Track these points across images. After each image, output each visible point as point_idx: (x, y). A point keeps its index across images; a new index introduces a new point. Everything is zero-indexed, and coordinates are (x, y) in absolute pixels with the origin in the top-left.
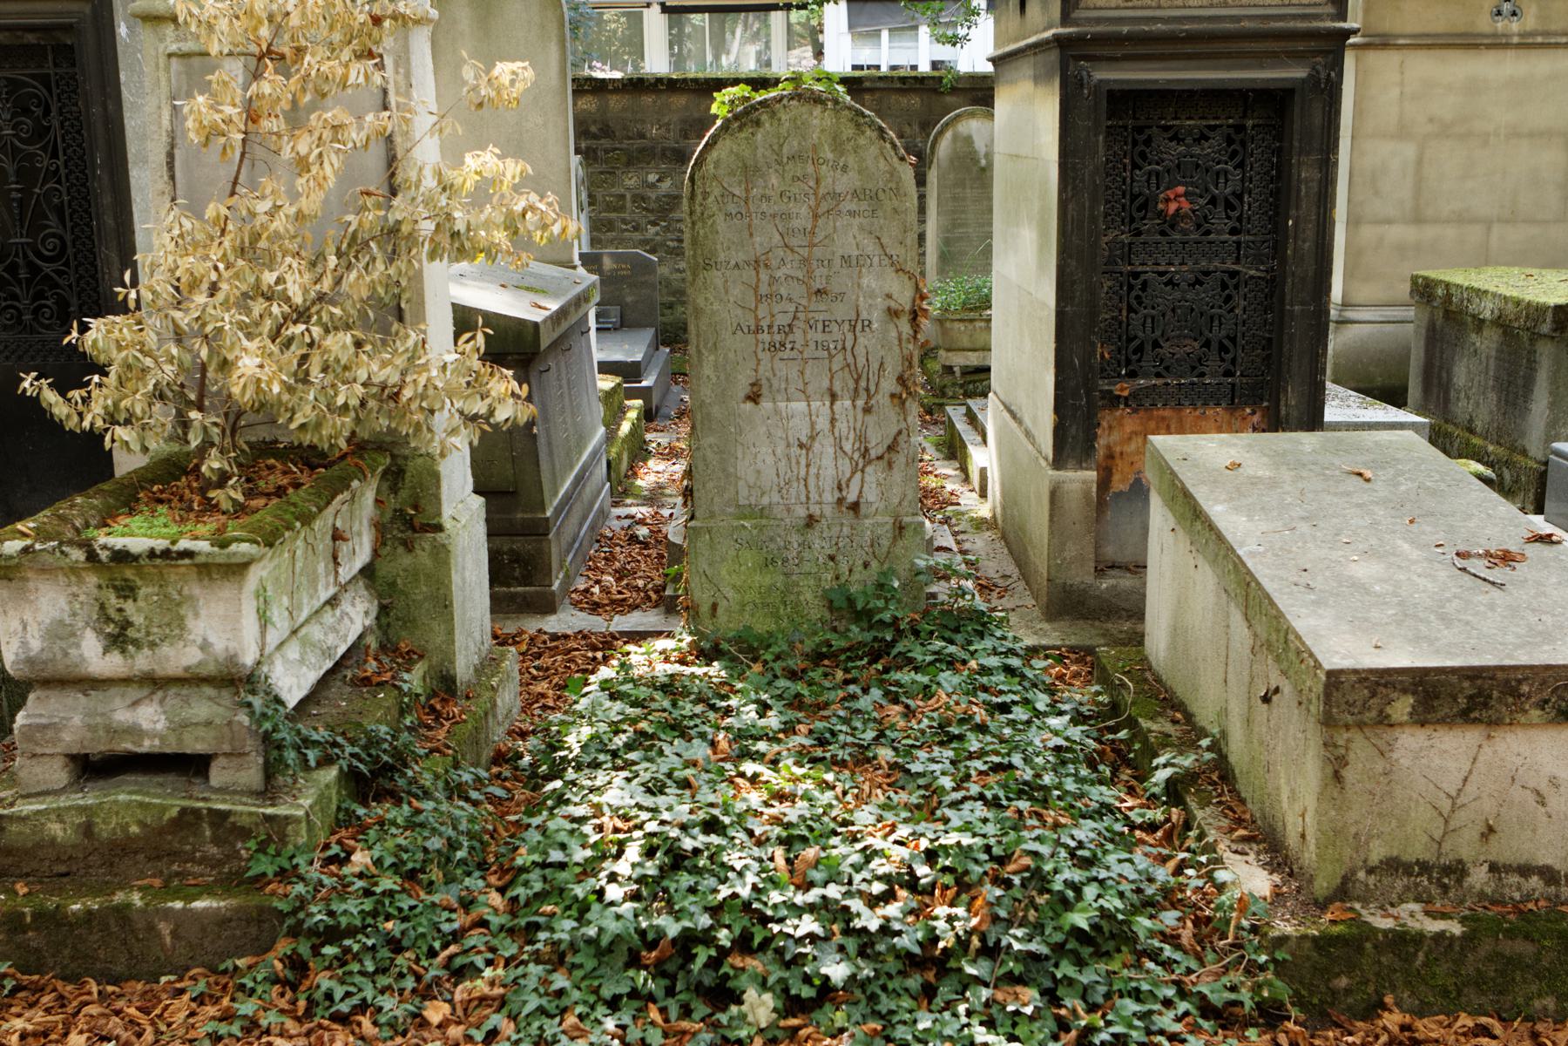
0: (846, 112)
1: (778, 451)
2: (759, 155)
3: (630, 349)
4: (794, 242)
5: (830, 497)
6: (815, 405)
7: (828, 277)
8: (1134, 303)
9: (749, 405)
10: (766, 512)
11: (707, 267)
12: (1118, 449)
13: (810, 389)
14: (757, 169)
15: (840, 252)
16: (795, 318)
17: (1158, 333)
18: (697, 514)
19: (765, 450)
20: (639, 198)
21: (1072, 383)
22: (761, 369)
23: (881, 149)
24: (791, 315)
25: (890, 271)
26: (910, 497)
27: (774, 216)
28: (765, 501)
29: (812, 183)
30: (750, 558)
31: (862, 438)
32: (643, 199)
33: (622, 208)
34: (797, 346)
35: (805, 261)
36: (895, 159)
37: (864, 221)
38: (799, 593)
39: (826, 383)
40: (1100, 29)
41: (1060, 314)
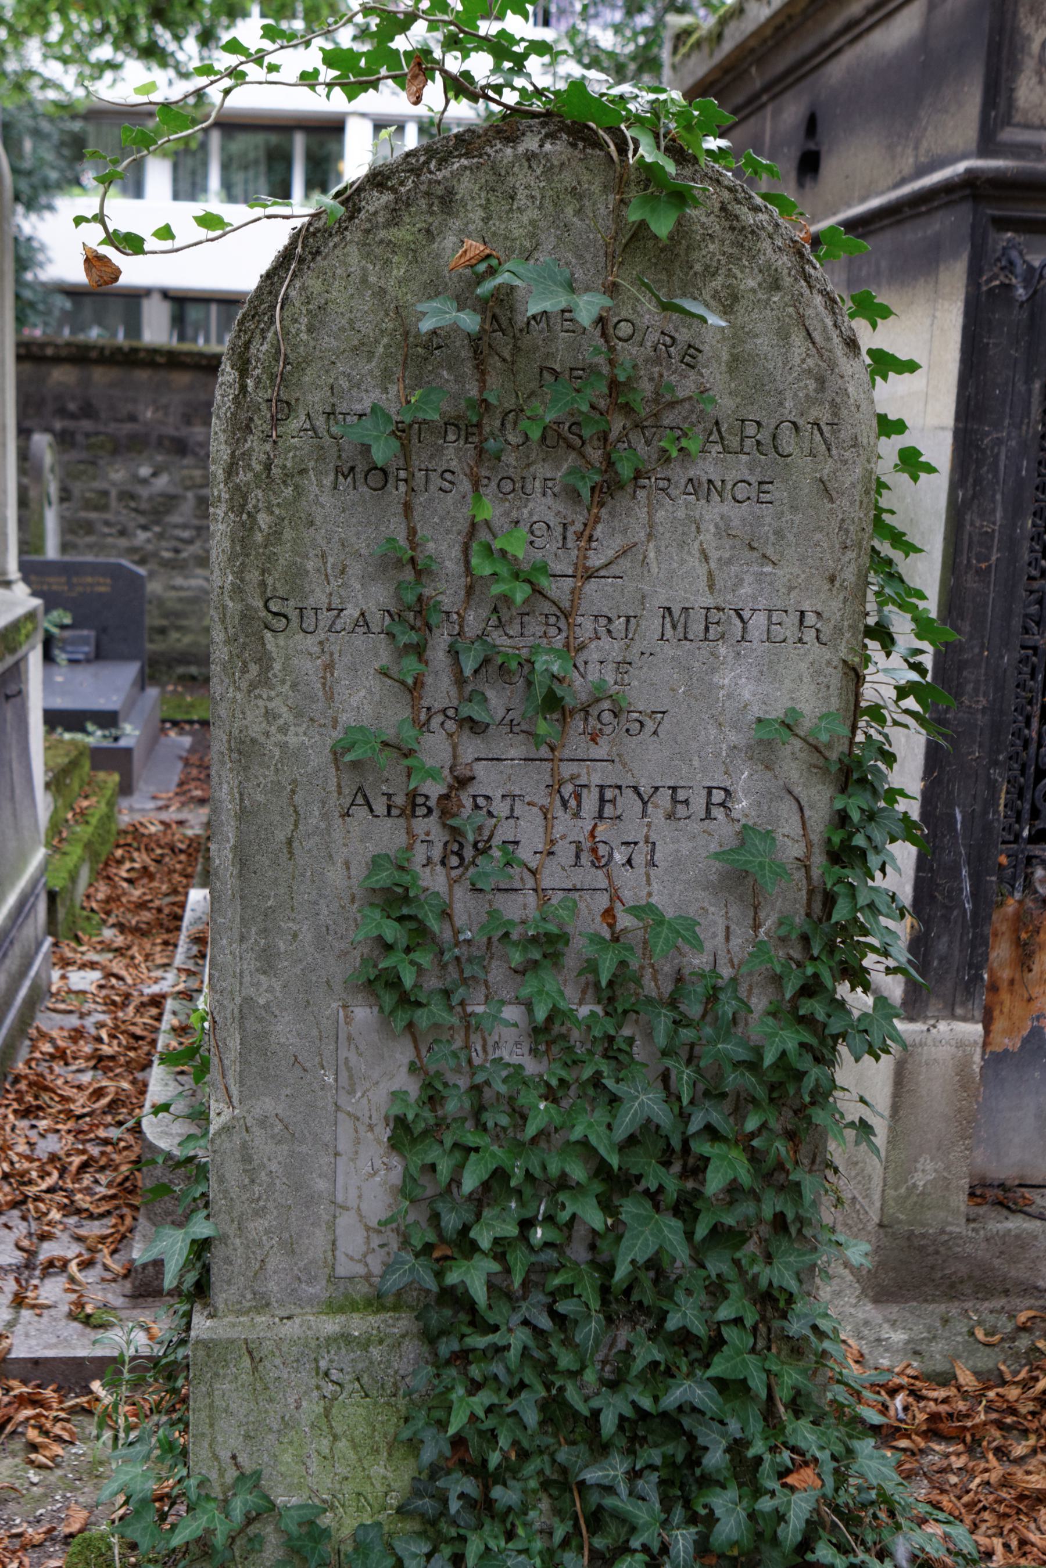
3: (106, 686)
7: (623, 665)
15: (662, 598)
20: (127, 496)
32: (132, 497)
33: (104, 508)
34: (524, 853)
37: (736, 514)
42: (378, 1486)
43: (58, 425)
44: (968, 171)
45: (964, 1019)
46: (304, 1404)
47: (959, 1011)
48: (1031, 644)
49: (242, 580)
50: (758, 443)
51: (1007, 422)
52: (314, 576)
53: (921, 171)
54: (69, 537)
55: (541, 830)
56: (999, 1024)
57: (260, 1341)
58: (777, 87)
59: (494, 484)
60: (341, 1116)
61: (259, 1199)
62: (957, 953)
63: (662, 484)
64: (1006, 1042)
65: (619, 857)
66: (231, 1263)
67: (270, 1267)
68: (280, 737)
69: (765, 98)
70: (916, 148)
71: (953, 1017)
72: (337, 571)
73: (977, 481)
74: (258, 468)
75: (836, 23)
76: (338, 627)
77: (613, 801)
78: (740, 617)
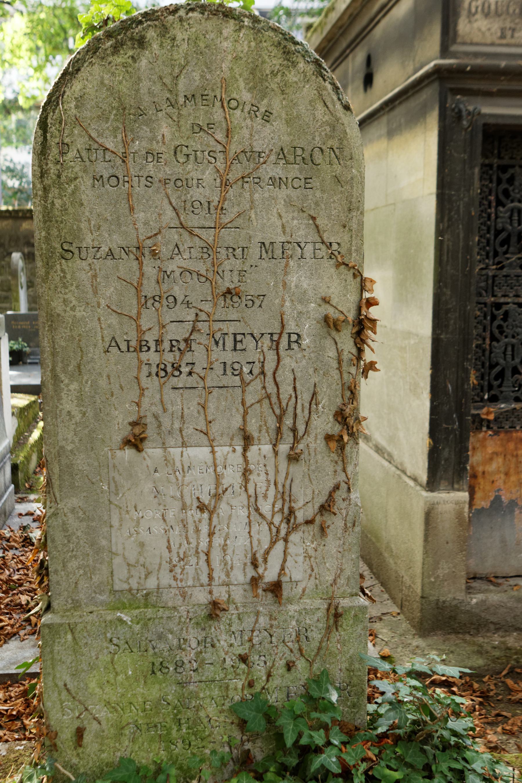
0: (271, 34)
1: (170, 515)
2: (144, 91)
4: (193, 221)
5: (241, 576)
6: (221, 451)
7: (242, 273)
8: (496, 332)
9: (129, 453)
10: (153, 599)
11: (66, 254)
12: (480, 469)
13: (215, 429)
14: (141, 113)
15: (259, 237)
16: (194, 330)
17: (517, 360)
18: (55, 604)
19: (151, 515)
21: (446, 408)
22: (146, 402)
23: (320, 90)
24: (189, 326)
25: (328, 265)
26: (348, 573)
27: (165, 182)
28: (151, 583)
29: (220, 136)
30: (129, 663)
31: (285, 495)
34: (198, 369)
35: (209, 249)
36: (338, 106)
37: (294, 194)
38: (198, 708)
39: (237, 422)
40: (479, 61)
41: (436, 342)
42: (140, 699)
43: (26, 250)
44: (435, 65)
45: (459, 490)
46: (100, 656)
47: (456, 486)
48: (483, 301)
49: (49, 234)
50: (303, 159)
51: (462, 189)
52: (85, 231)
53: (416, 71)
54: (33, 305)
55: (205, 357)
56: (478, 495)
57: (76, 624)
58: (353, 45)
59: (172, 183)
60: (112, 507)
61: (73, 551)
62: (453, 457)
63: (256, 180)
64: (482, 503)
65: (246, 370)
66: (60, 585)
67: (80, 586)
68: (72, 313)
69: (348, 51)
70: (414, 60)
71: (453, 489)
72: (96, 229)
73: (450, 219)
74: (54, 177)
75: (376, 7)
76: (98, 257)
77: (241, 341)
78: (300, 246)
